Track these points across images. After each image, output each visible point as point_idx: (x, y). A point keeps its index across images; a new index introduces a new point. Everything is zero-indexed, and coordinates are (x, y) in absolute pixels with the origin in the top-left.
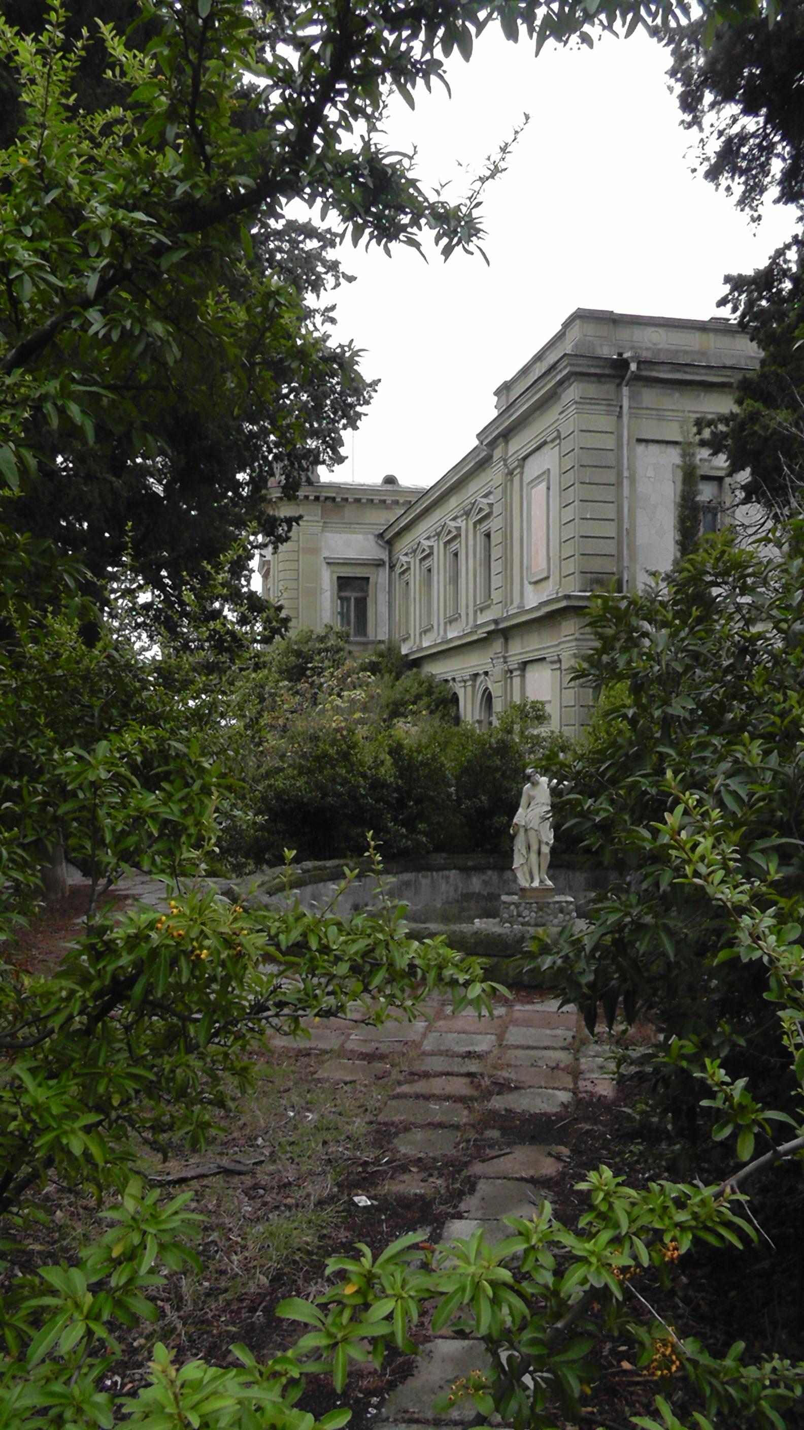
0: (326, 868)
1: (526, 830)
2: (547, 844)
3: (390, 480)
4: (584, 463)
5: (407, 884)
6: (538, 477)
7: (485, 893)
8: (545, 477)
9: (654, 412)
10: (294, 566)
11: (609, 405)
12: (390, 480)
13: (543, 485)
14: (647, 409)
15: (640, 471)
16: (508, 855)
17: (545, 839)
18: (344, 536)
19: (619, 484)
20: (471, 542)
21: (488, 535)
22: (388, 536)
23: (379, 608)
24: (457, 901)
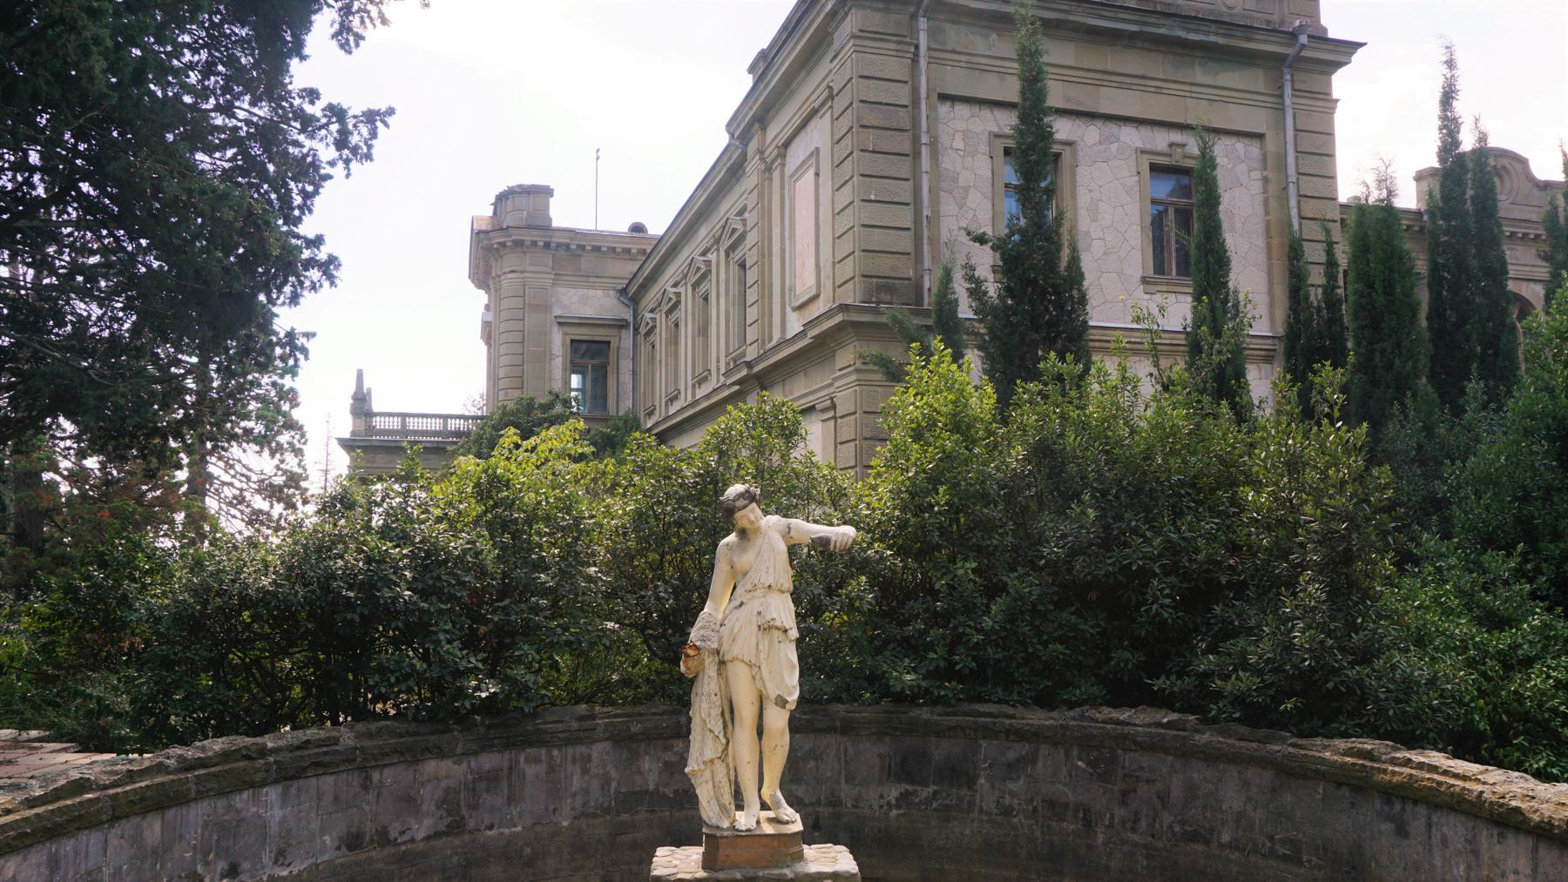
0: (263, 752)
1: (722, 663)
2: (781, 702)
3: (638, 228)
4: (865, 122)
5: (491, 779)
6: (804, 162)
7: (669, 792)
8: (813, 160)
9: (963, 58)
10: (518, 326)
11: (899, 43)
12: (638, 228)
13: (812, 172)
14: (954, 52)
15: (944, 140)
16: (801, 658)
17: (773, 692)
18: (582, 292)
19: (916, 154)
20: (722, 276)
21: (743, 266)
22: (632, 290)
23: (621, 377)
24: (607, 811)
